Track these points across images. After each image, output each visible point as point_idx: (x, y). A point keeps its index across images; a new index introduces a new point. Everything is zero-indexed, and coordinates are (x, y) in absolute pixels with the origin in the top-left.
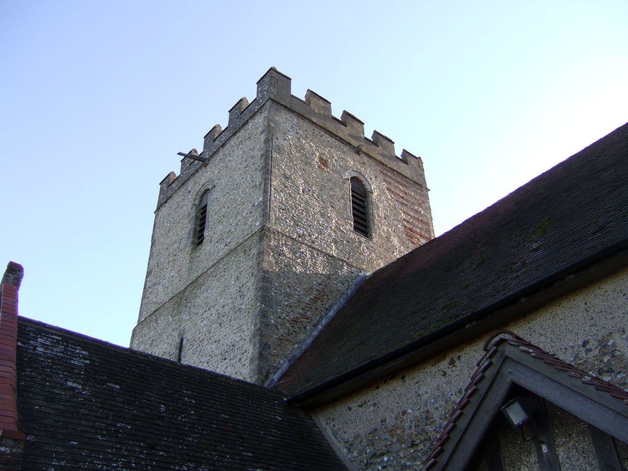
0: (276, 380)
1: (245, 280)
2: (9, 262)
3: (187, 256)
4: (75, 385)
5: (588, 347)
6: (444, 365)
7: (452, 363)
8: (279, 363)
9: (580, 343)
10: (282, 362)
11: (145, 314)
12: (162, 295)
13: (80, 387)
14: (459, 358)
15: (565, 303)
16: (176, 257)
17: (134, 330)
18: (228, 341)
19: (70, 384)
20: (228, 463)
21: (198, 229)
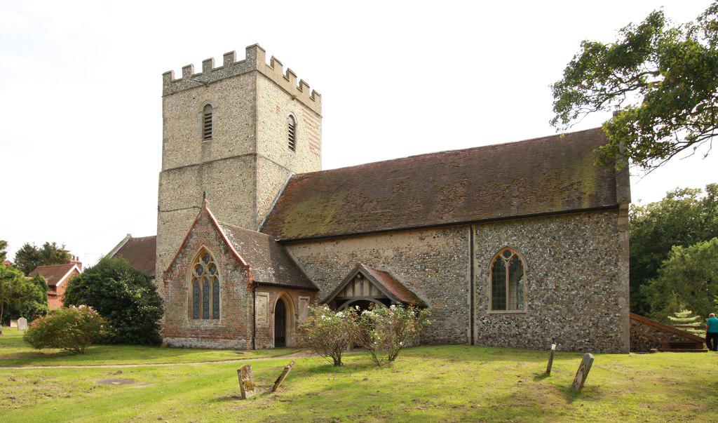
6: (334, 243)
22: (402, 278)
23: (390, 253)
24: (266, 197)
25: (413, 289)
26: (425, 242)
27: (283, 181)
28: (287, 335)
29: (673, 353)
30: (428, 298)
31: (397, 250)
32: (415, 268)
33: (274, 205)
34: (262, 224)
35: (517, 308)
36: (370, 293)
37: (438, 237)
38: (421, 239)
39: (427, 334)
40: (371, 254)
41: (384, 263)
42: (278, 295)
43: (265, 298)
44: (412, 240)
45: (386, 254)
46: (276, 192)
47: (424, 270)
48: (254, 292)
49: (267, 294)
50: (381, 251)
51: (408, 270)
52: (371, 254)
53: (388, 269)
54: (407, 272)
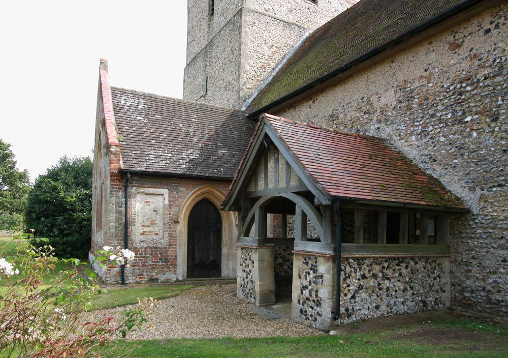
0: (250, 102)
1: (234, 44)
2: (62, 156)
3: (207, 24)
4: (140, 118)
5: (363, 100)
6: (310, 102)
7: (314, 102)
8: (252, 93)
9: (361, 98)
10: (253, 92)
11: (190, 60)
12: (196, 49)
13: (143, 119)
14: (316, 100)
15: (378, 69)
16: (201, 23)
17: (185, 69)
18: (227, 80)
19: (138, 118)
20: (209, 148)
21: (211, 4)
22: (411, 148)
23: (389, 98)
24: (260, 65)
25: (436, 171)
26: (463, 52)
27: (291, 43)
28: (223, 258)
29: (269, 135)
30: (473, 189)
31: (401, 89)
32: (440, 120)
33: (274, 73)
34: (250, 100)
35: (122, 207)
36: (288, 182)
37: (497, 26)
38: (455, 46)
39: (468, 283)
40: (359, 109)
41: (379, 121)
42: (188, 197)
43: (160, 198)
44: (433, 57)
45: (383, 101)
46: (278, 57)
47: (461, 122)
48: (126, 187)
49: (165, 192)
50: (374, 99)
51: (425, 126)
52: (359, 109)
53: (387, 132)
54: (424, 133)
